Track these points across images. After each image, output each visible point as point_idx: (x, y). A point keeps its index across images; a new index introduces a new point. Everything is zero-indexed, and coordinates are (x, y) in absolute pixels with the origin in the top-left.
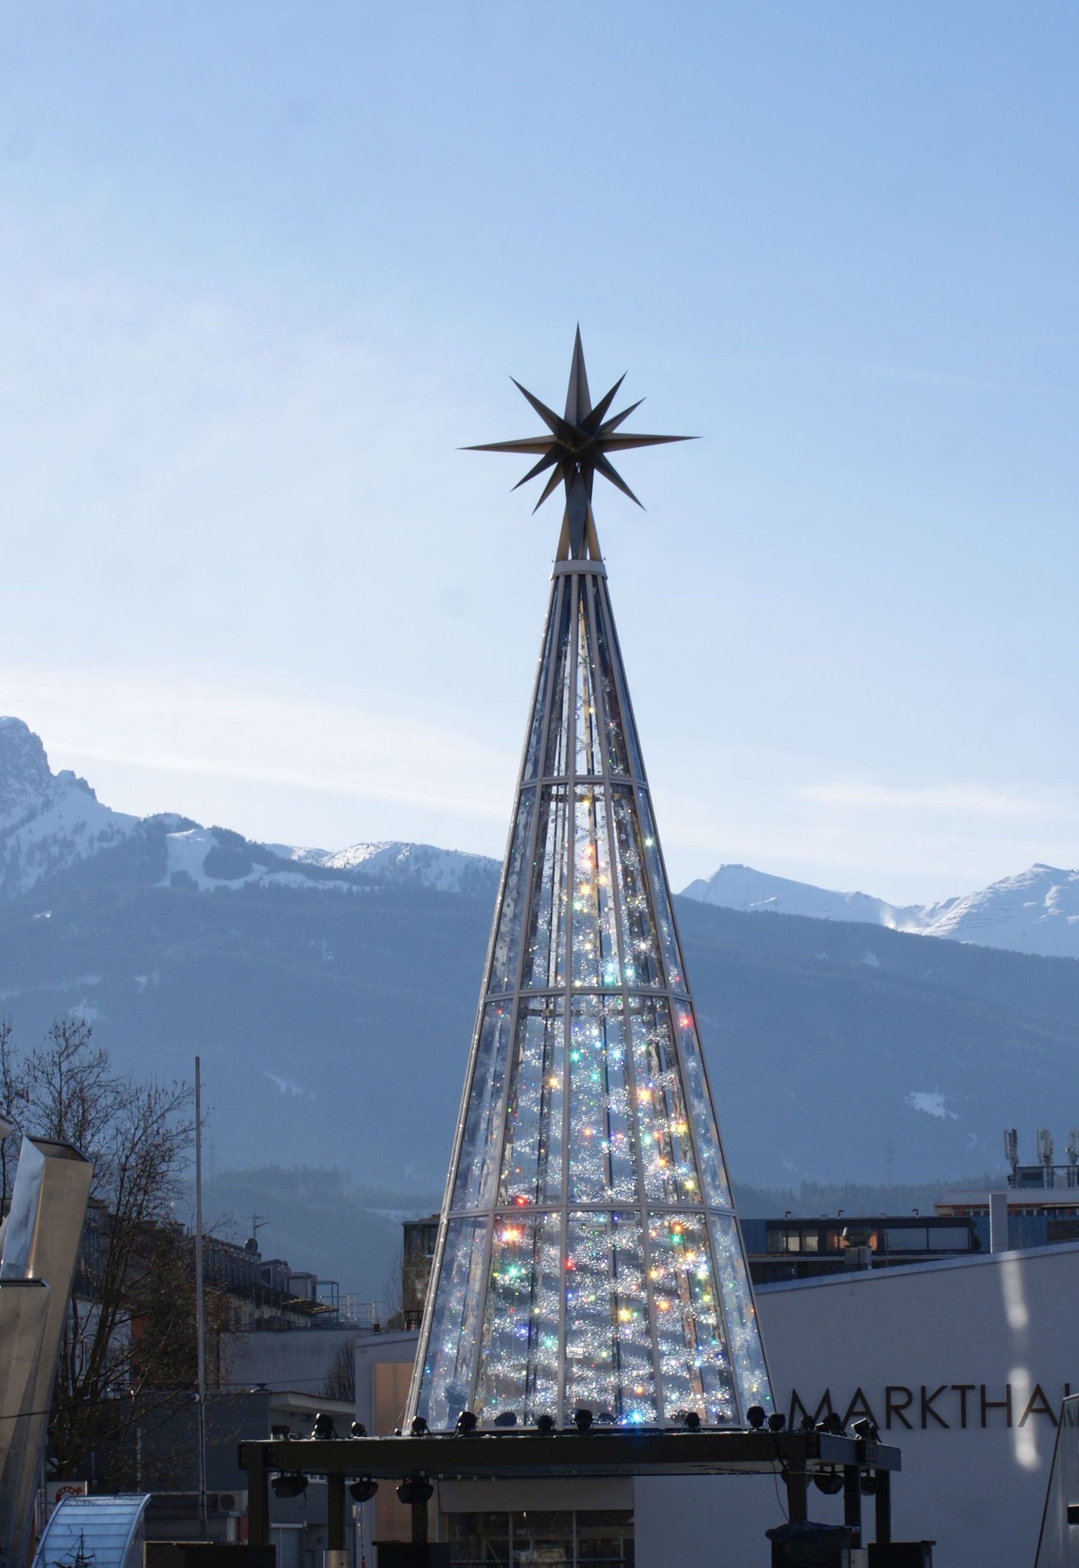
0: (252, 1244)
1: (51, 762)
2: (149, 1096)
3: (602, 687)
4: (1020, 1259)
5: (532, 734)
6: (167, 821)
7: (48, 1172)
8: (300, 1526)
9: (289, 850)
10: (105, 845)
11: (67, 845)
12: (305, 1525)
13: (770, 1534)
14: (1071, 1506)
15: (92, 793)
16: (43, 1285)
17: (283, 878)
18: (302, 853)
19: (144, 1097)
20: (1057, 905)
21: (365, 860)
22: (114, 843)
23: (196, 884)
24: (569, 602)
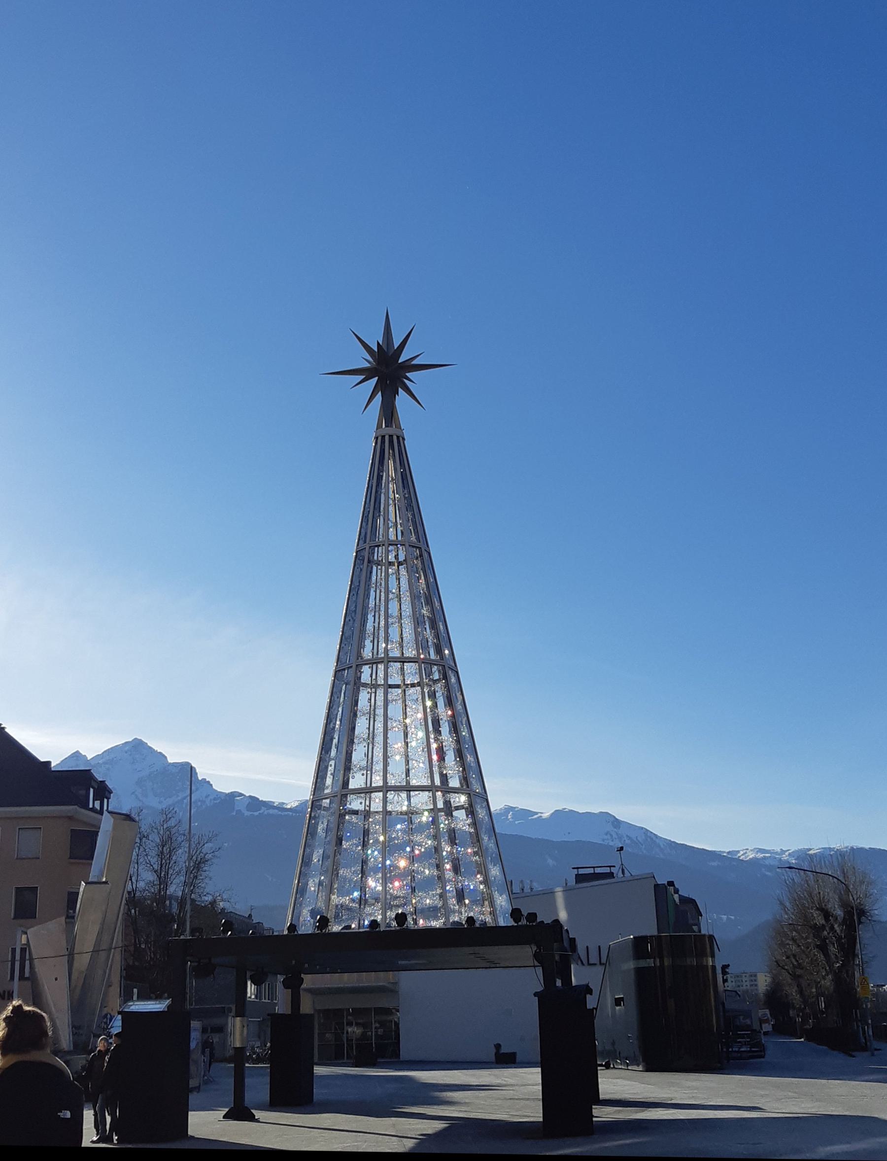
0: (250, 916)
1: (199, 776)
2: (199, 837)
3: (404, 494)
4: (563, 891)
5: (363, 522)
6: (235, 794)
7: (115, 828)
8: (259, 1020)
9: (274, 803)
10: (215, 802)
11: (203, 802)
12: (262, 1019)
13: (536, 994)
14: (616, 997)
15: (211, 785)
16: (108, 884)
17: (271, 811)
18: (277, 803)
19: (197, 837)
20: (512, 818)
21: (297, 806)
22: (218, 801)
23: (244, 814)
24: (384, 450)
